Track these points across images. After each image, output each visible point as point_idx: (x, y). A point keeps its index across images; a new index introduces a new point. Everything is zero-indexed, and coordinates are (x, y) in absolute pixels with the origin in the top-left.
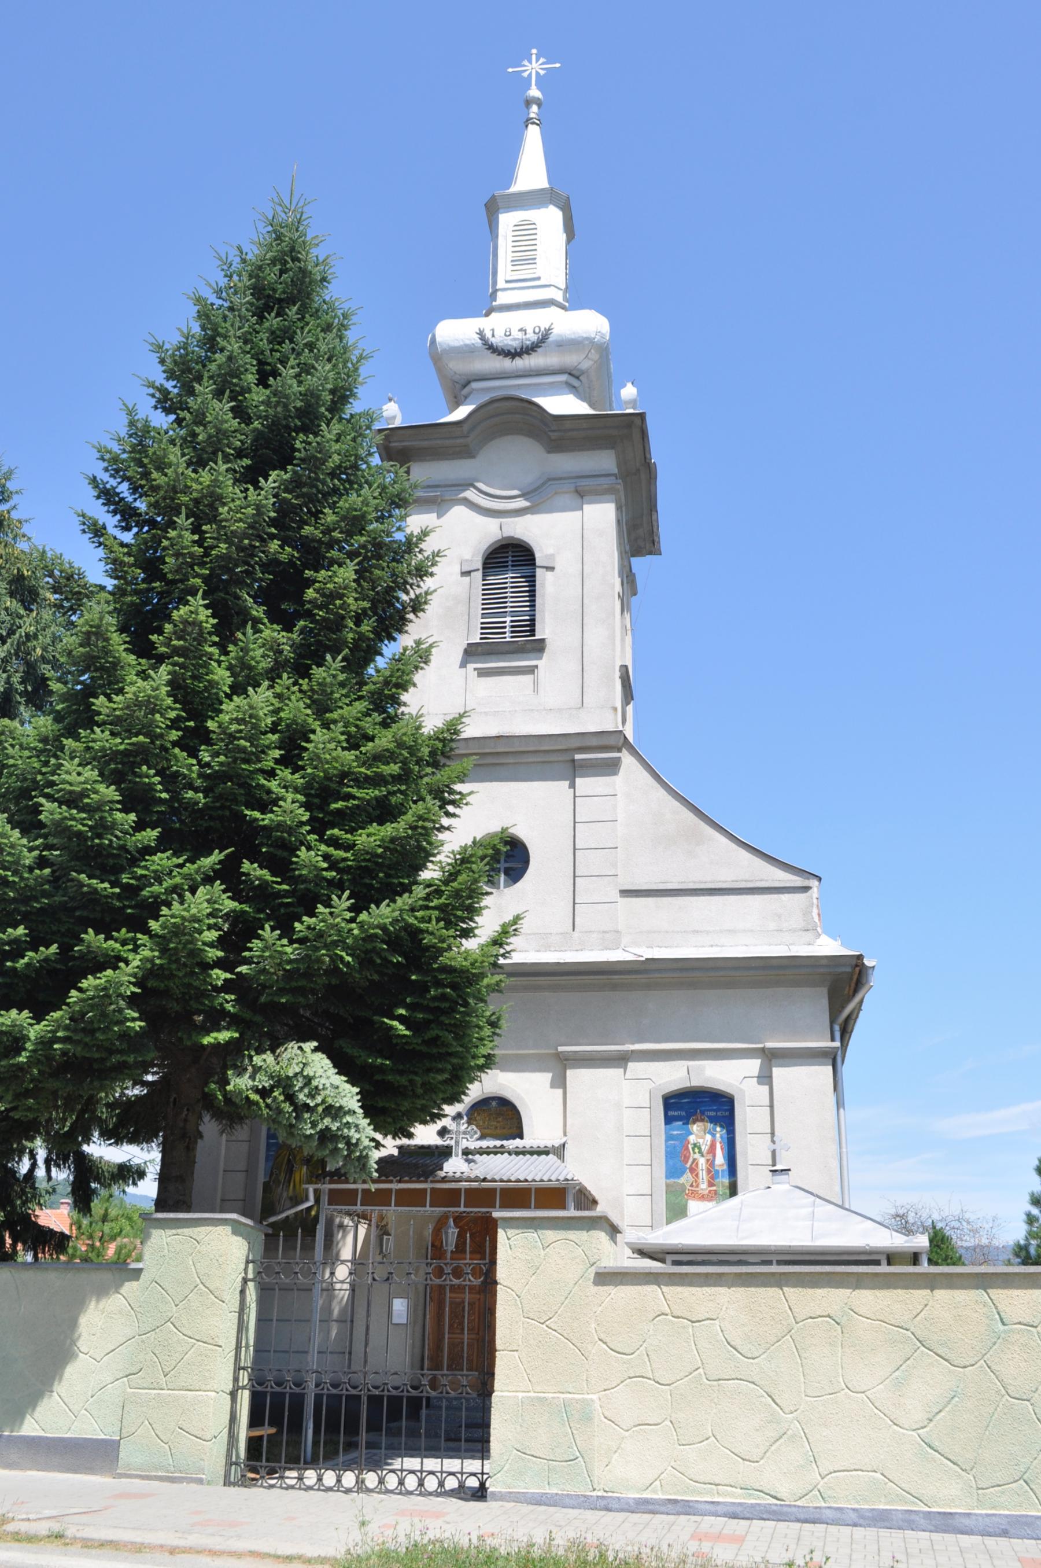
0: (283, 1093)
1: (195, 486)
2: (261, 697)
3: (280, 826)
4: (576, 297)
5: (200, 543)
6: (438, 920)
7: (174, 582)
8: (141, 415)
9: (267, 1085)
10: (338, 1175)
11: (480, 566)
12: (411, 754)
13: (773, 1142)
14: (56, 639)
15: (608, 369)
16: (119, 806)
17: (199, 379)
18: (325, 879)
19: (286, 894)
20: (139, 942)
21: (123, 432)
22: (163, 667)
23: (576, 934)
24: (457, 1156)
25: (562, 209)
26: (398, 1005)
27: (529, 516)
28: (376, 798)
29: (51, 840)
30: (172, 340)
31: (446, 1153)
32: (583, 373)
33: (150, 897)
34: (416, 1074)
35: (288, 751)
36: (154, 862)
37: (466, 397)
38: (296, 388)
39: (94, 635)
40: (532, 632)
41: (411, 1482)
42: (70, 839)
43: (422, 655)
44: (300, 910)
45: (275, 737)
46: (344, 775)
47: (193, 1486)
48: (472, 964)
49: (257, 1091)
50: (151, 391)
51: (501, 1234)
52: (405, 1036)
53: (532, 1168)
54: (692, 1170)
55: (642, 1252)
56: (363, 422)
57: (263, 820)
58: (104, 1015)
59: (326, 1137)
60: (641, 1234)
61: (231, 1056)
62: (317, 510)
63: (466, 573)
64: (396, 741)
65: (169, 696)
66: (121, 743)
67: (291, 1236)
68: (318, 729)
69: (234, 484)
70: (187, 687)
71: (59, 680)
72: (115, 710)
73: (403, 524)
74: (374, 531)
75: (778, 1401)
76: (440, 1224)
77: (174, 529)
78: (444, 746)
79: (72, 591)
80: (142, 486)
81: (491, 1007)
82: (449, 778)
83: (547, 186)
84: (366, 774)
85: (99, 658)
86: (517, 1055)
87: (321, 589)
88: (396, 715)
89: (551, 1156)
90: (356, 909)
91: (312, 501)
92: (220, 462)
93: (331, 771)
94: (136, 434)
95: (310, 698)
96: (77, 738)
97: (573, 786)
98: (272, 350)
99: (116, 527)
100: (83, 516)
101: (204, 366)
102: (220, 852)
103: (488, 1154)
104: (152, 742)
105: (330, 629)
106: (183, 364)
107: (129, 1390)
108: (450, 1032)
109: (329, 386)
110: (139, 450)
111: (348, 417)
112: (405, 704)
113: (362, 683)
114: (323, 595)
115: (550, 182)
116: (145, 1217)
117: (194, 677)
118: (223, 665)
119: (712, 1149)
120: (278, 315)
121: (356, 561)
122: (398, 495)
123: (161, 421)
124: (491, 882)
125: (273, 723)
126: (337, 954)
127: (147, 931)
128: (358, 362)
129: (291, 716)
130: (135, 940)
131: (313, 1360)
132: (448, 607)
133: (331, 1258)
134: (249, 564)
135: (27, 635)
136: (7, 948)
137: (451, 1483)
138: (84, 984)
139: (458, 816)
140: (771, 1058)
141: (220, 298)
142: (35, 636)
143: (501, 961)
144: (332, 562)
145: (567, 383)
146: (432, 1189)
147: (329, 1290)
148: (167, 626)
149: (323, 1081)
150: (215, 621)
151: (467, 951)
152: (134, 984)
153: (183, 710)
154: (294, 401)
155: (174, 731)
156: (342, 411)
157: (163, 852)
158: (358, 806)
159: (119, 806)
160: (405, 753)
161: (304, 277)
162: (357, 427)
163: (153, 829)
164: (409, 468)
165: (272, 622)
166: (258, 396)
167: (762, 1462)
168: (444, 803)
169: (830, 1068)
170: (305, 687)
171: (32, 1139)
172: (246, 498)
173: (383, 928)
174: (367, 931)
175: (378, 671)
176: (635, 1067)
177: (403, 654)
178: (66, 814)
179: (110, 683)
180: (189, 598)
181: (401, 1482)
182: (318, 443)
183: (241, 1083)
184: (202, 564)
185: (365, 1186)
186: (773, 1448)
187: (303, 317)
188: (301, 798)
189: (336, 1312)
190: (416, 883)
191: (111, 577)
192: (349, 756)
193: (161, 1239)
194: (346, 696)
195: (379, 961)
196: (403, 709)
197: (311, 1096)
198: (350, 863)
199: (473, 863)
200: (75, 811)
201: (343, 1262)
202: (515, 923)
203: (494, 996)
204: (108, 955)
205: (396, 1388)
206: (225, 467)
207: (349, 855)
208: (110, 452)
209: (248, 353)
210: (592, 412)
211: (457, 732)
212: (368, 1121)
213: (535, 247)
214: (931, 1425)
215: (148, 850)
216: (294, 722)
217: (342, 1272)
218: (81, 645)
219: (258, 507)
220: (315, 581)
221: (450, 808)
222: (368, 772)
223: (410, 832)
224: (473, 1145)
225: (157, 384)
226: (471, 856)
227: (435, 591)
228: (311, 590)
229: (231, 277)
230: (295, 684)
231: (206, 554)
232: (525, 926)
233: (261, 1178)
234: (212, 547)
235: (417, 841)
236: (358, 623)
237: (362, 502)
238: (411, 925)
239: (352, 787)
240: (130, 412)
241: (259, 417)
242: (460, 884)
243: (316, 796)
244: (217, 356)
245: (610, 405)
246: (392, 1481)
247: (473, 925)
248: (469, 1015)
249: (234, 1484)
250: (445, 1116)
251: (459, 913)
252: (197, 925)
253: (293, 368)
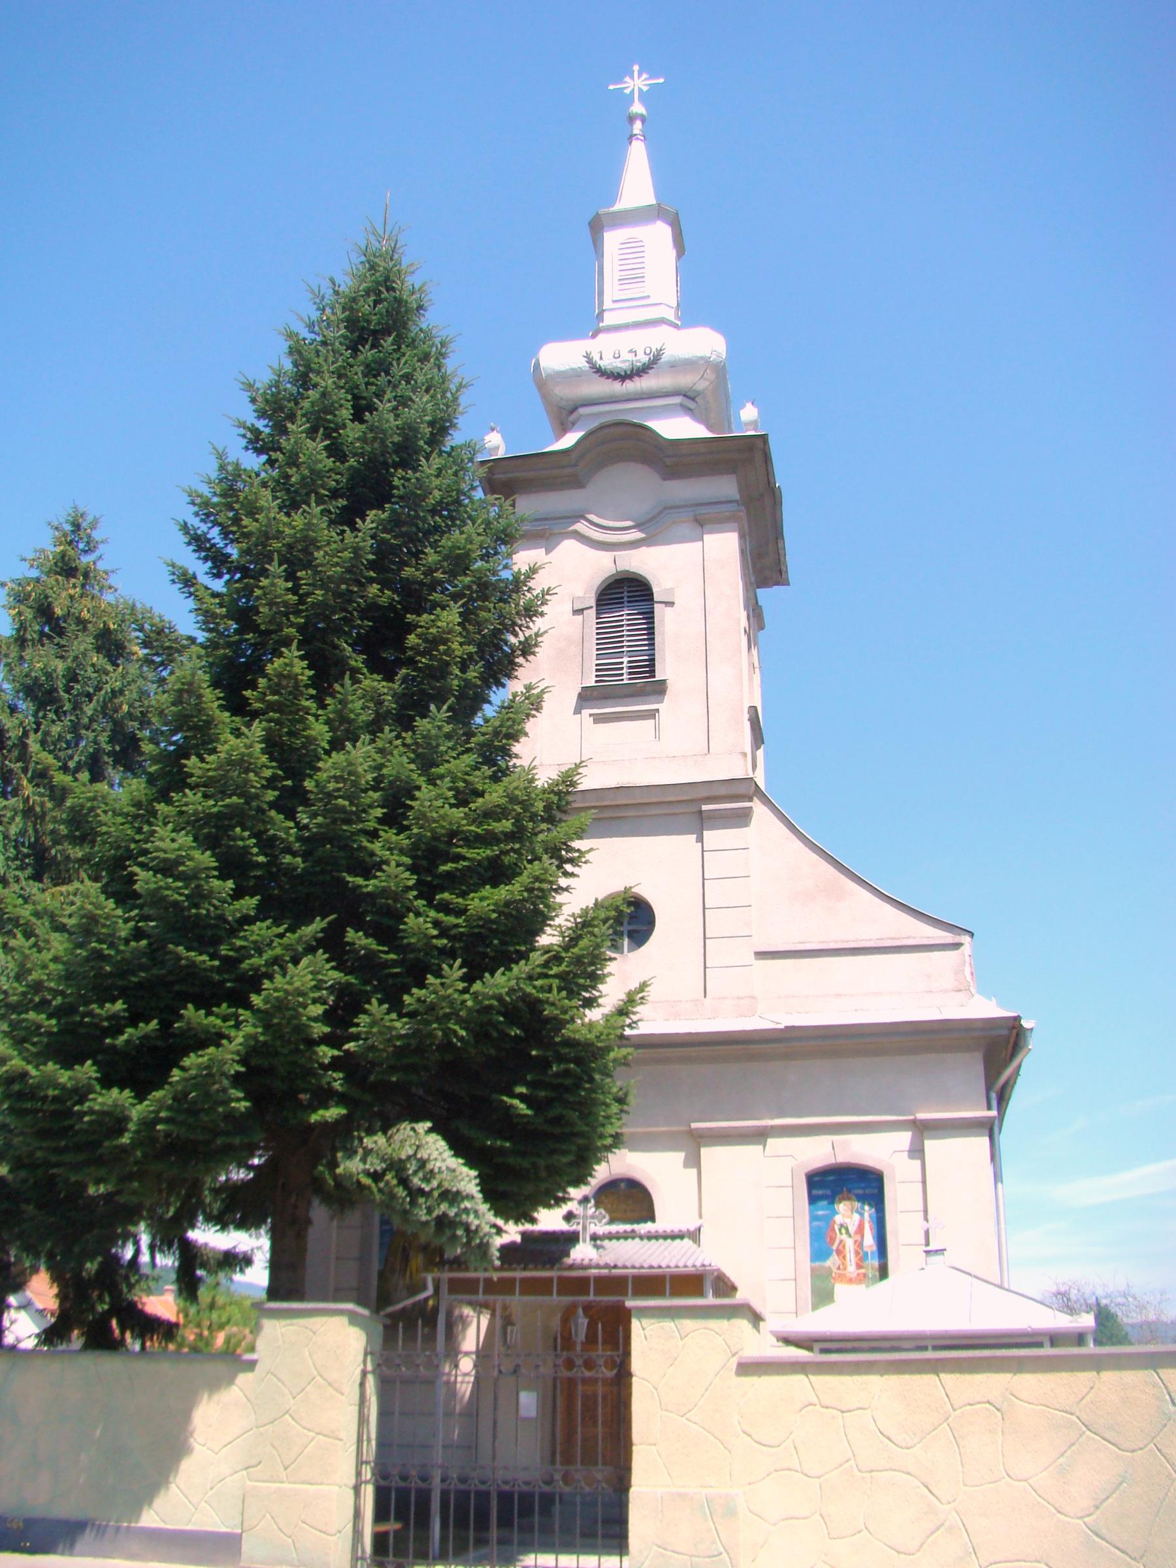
0: (396, 1176)
1: (287, 531)
3: (384, 892)
4: (690, 313)
5: (294, 590)
6: (560, 989)
7: (268, 633)
8: (232, 458)
9: (379, 1168)
10: (458, 1263)
11: (593, 604)
13: (926, 1219)
15: (726, 388)
16: (216, 873)
17: (292, 417)
18: (436, 947)
19: (394, 963)
20: (241, 1018)
21: (214, 475)
22: (256, 723)
23: (707, 1001)
24: (584, 1241)
25: (671, 225)
26: (517, 1083)
27: (644, 548)
28: (488, 858)
29: (147, 911)
30: (264, 378)
31: (572, 1239)
32: (699, 394)
35: (394, 810)
36: (253, 932)
37: (573, 424)
39: (188, 690)
40: (652, 673)
42: (166, 909)
43: (534, 702)
45: (376, 795)
46: (453, 834)
49: (368, 1173)
50: (242, 431)
51: (635, 1324)
52: (526, 1116)
53: (666, 1253)
54: (839, 1252)
55: (787, 1340)
57: (367, 886)
58: (207, 1095)
59: (443, 1223)
61: (340, 1136)
62: (418, 550)
63: (578, 612)
64: (507, 796)
65: (264, 753)
66: (214, 806)
67: (410, 1327)
68: (424, 786)
69: (329, 526)
72: (208, 770)
74: (479, 570)
76: (568, 1315)
77: (267, 577)
78: (560, 800)
79: (162, 644)
80: (234, 533)
81: (619, 1083)
84: (476, 833)
85: (192, 716)
86: (647, 1133)
87: (423, 634)
88: (508, 768)
89: (686, 1240)
90: (469, 979)
91: (411, 540)
93: (438, 830)
95: (414, 751)
96: (169, 802)
97: (700, 839)
98: (367, 384)
99: (207, 573)
100: (173, 566)
101: (297, 403)
102: (322, 919)
103: (618, 1238)
104: (247, 803)
105: (434, 677)
106: (275, 403)
107: (249, 1483)
108: (575, 1110)
109: (427, 418)
111: (448, 449)
112: (517, 756)
113: (470, 735)
114: (426, 641)
115: (657, 196)
116: (257, 1306)
118: (322, 719)
119: (860, 1229)
121: (460, 603)
122: (504, 531)
123: (253, 462)
124: (616, 947)
125: (374, 779)
126: (450, 1029)
127: (248, 1006)
128: (458, 390)
129: (394, 772)
130: (237, 1016)
131: (438, 1455)
132: (560, 649)
133: (453, 1353)
135: (113, 691)
138: (186, 1062)
139: (577, 876)
140: (923, 1130)
141: (313, 332)
142: (121, 692)
143: (628, 1032)
144: (435, 605)
145: (681, 405)
146: (560, 1279)
147: (451, 1387)
148: (260, 680)
149: (438, 1164)
152: (238, 1062)
153: (279, 768)
154: (391, 436)
155: (270, 791)
156: (442, 443)
157: (263, 920)
159: (216, 873)
161: (400, 306)
162: (458, 461)
163: (252, 897)
164: (514, 501)
166: (353, 432)
167: (918, 1554)
168: (563, 861)
169: (987, 1139)
170: (409, 741)
171: (136, 1224)
173: (499, 998)
174: (481, 1002)
175: (487, 721)
177: (513, 701)
178: (162, 883)
179: (204, 743)
180: (283, 649)
183: (352, 1166)
184: (297, 613)
185: (487, 1275)
186: (931, 1539)
187: (399, 348)
188: (407, 860)
190: (534, 949)
191: (203, 630)
192: (458, 813)
194: (452, 749)
196: (515, 761)
197: (427, 1179)
198: (461, 930)
199: (595, 926)
200: (170, 880)
201: (467, 1354)
202: (642, 991)
204: (209, 1032)
205: (527, 1483)
206: (319, 508)
207: (460, 921)
208: (201, 496)
209: (342, 388)
210: (710, 435)
211: (573, 784)
212: (487, 1206)
213: (642, 267)
214: (1098, 1512)
215: (247, 920)
216: (398, 778)
217: (467, 1364)
218: (173, 704)
219: (356, 550)
220: (417, 626)
221: (568, 867)
222: (479, 831)
223: (526, 894)
224: (601, 1228)
225: (248, 424)
226: (593, 919)
227: (546, 632)
228: (413, 636)
229: (324, 310)
230: (398, 737)
231: (302, 601)
232: (652, 993)
233: (376, 1266)
234: (308, 594)
236: (464, 669)
237: (466, 539)
238: (530, 995)
239: (461, 847)
240: (220, 456)
241: (355, 455)
242: (581, 949)
244: (310, 392)
247: (597, 994)
250: (571, 1199)
251: (581, 981)
252: (301, 999)
253: (389, 401)
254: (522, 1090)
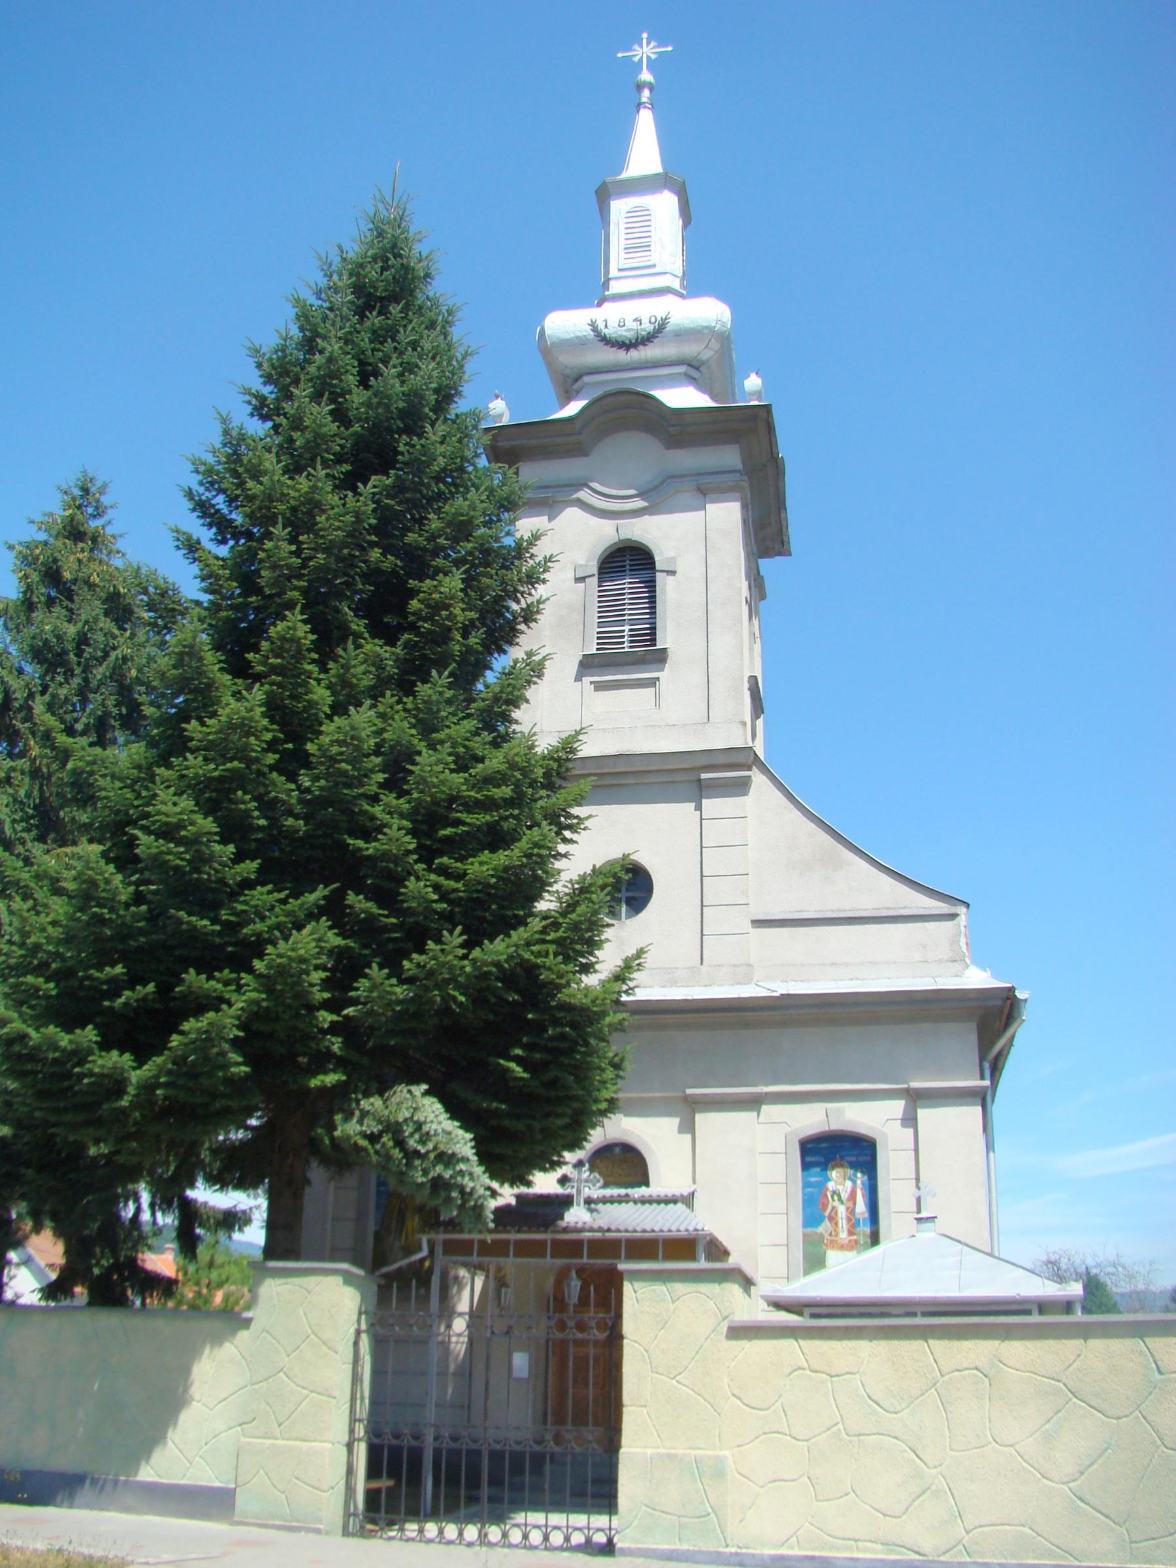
1: (292, 493)
2: (363, 717)
3: (385, 856)
4: (695, 283)
5: (297, 553)
6: (556, 954)
7: (271, 596)
9: (375, 1130)
10: (452, 1225)
11: (595, 571)
12: (525, 775)
13: (918, 1187)
14: (151, 659)
16: (217, 838)
18: (436, 912)
20: (243, 982)
24: (578, 1204)
28: (487, 823)
29: (147, 875)
30: (269, 342)
31: (565, 1202)
32: (703, 363)
33: (252, 935)
34: (534, 1118)
35: (393, 774)
36: (253, 896)
37: (578, 392)
38: (398, 388)
39: (188, 654)
40: (653, 641)
41: (536, 1537)
43: (536, 670)
44: (410, 945)
46: (452, 799)
47: (312, 1536)
48: (593, 1001)
49: (365, 1136)
50: (247, 398)
51: (627, 1287)
52: (522, 1079)
54: (832, 1219)
55: (778, 1305)
56: (470, 422)
57: (367, 849)
58: (207, 1058)
59: (438, 1184)
60: (777, 1286)
64: (508, 762)
66: (215, 769)
67: (404, 1287)
68: (424, 750)
70: (285, 707)
71: (152, 704)
72: (209, 734)
73: (512, 528)
74: (482, 536)
75: (922, 1456)
76: (562, 1276)
77: (271, 540)
78: (560, 766)
79: (166, 608)
81: (614, 1048)
82: (565, 801)
83: (660, 170)
84: (476, 798)
88: (507, 734)
89: (679, 1205)
90: (469, 945)
91: (415, 507)
92: (319, 467)
94: (230, 443)
95: (415, 717)
96: (169, 766)
97: (699, 807)
98: (373, 350)
99: (212, 540)
100: (177, 531)
102: (326, 887)
103: (612, 1202)
104: (248, 767)
108: (570, 1074)
109: (433, 385)
110: (235, 458)
112: (517, 722)
113: (470, 700)
114: (428, 606)
117: (293, 697)
119: (853, 1196)
120: (380, 314)
122: (507, 499)
123: (258, 428)
124: (613, 914)
125: (376, 744)
127: (251, 970)
128: (464, 358)
129: (395, 737)
130: (237, 981)
131: (431, 1414)
132: (561, 616)
133: (447, 1313)
134: (348, 575)
136: (105, 987)
137: (578, 1538)
138: (186, 1026)
139: (576, 842)
140: (916, 1098)
141: (320, 299)
143: (624, 998)
144: (438, 570)
145: (686, 375)
146: (554, 1241)
147: (445, 1345)
148: (264, 643)
149: (434, 1126)
150: (315, 637)
151: (587, 988)
154: (396, 402)
157: (263, 884)
158: (468, 833)
159: (217, 838)
160: (518, 775)
161: (407, 273)
162: (463, 428)
163: (253, 860)
165: (373, 636)
166: (358, 397)
167: (904, 1517)
168: (562, 827)
169: (980, 1108)
170: (410, 706)
172: (344, 505)
173: (497, 964)
175: (487, 687)
176: (769, 1111)
177: (514, 667)
178: (164, 848)
181: (525, 1536)
182: (422, 446)
183: (349, 1129)
184: (300, 577)
185: (482, 1237)
187: (407, 315)
188: (406, 823)
189: (452, 1367)
190: (532, 914)
192: (458, 778)
193: (273, 1289)
194: (454, 714)
195: (493, 1000)
196: (514, 726)
197: (422, 1142)
198: (461, 894)
199: (593, 892)
200: (172, 845)
201: (461, 1314)
202: (639, 957)
203: (615, 1035)
205: (518, 1443)
208: (204, 464)
211: (573, 751)
212: (482, 1169)
213: (649, 235)
214: (1083, 1478)
216: (398, 743)
217: (460, 1325)
218: (175, 667)
219: (357, 514)
221: (567, 834)
222: (479, 796)
223: (524, 860)
224: (596, 1192)
226: (591, 885)
227: (548, 599)
229: (331, 276)
230: (399, 702)
232: (649, 960)
233: (372, 1227)
235: (534, 871)
237: (469, 506)
239: (461, 812)
240: (224, 421)
241: (359, 420)
242: (579, 915)
243: (422, 822)
244: (317, 356)
245: (733, 395)
246: (516, 1536)
247: (594, 960)
248: (591, 1055)
249: (353, 1535)
250: (566, 1163)
251: (578, 947)
253: (395, 367)
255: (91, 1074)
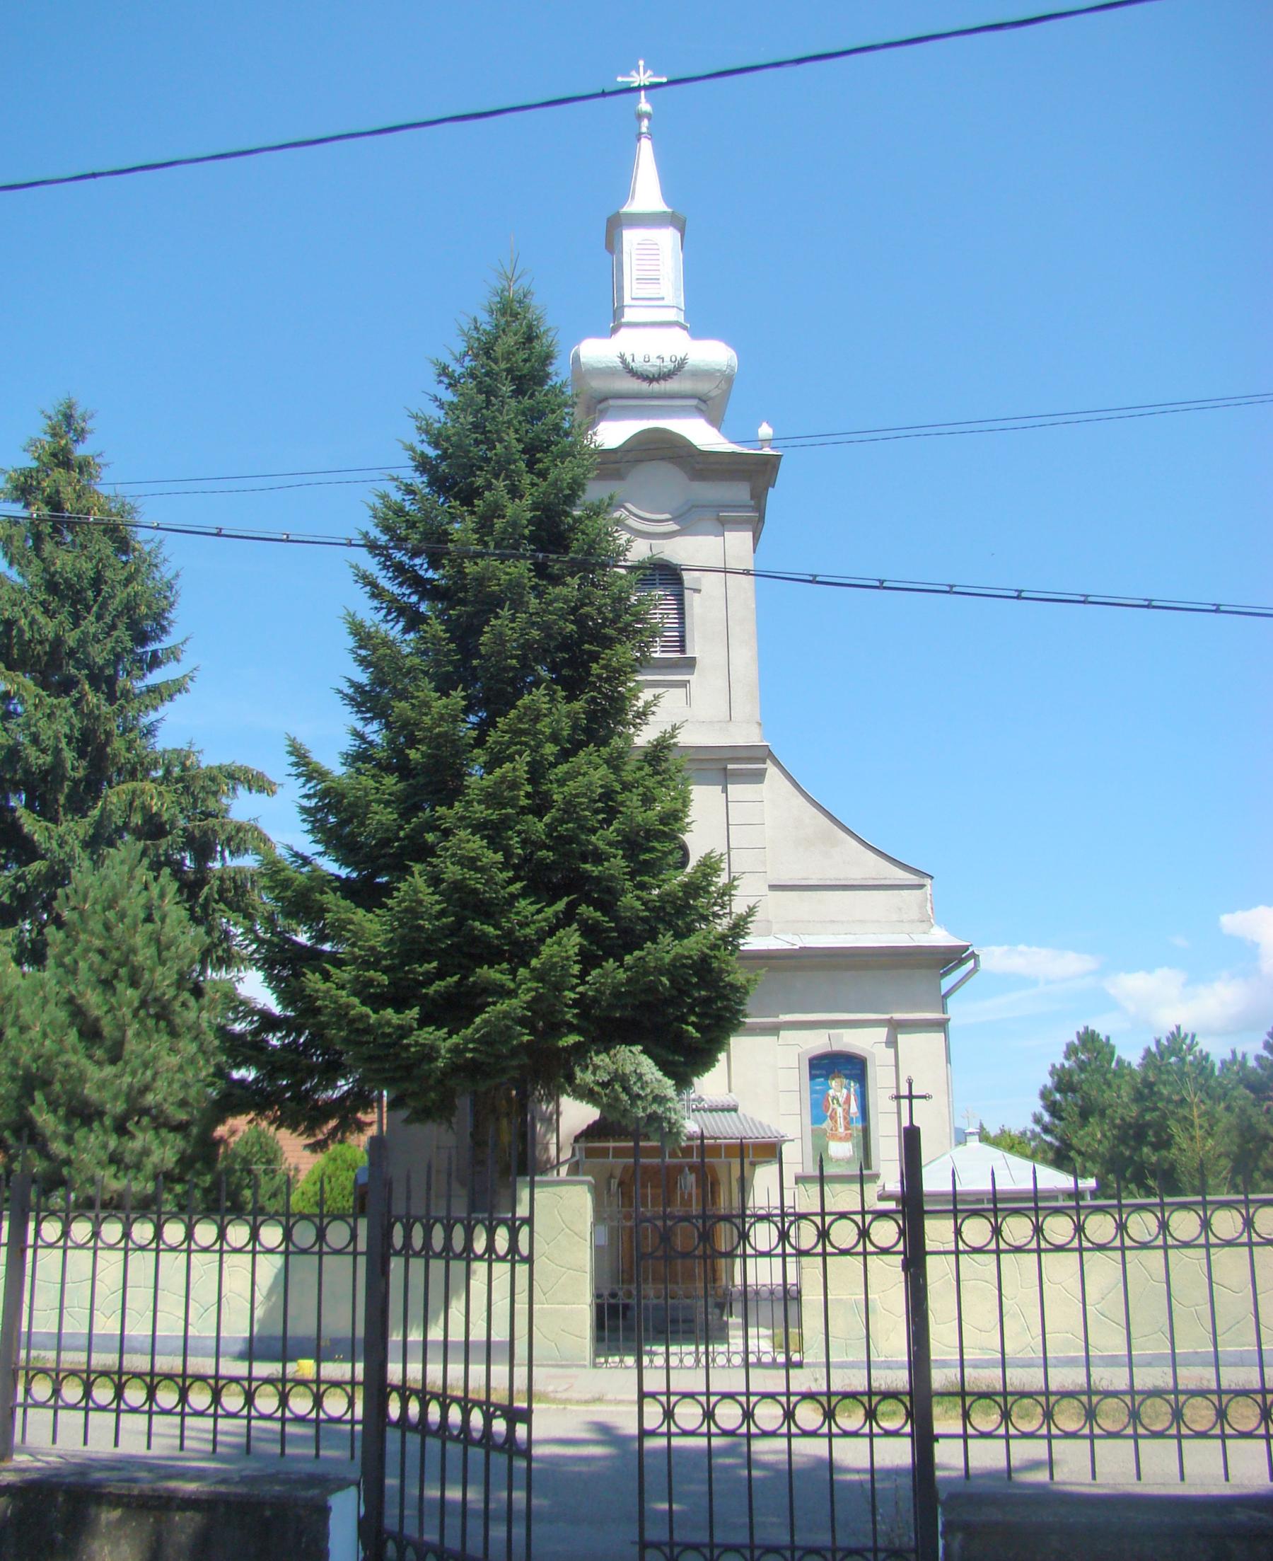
32: (711, 398)
40: (682, 649)
49: (598, 1083)
54: (833, 1118)
97: (725, 791)
119: (848, 1101)
140: (896, 1027)
197: (642, 1088)
213: (653, 263)
254: (693, 1019)
255: (417, 1044)
